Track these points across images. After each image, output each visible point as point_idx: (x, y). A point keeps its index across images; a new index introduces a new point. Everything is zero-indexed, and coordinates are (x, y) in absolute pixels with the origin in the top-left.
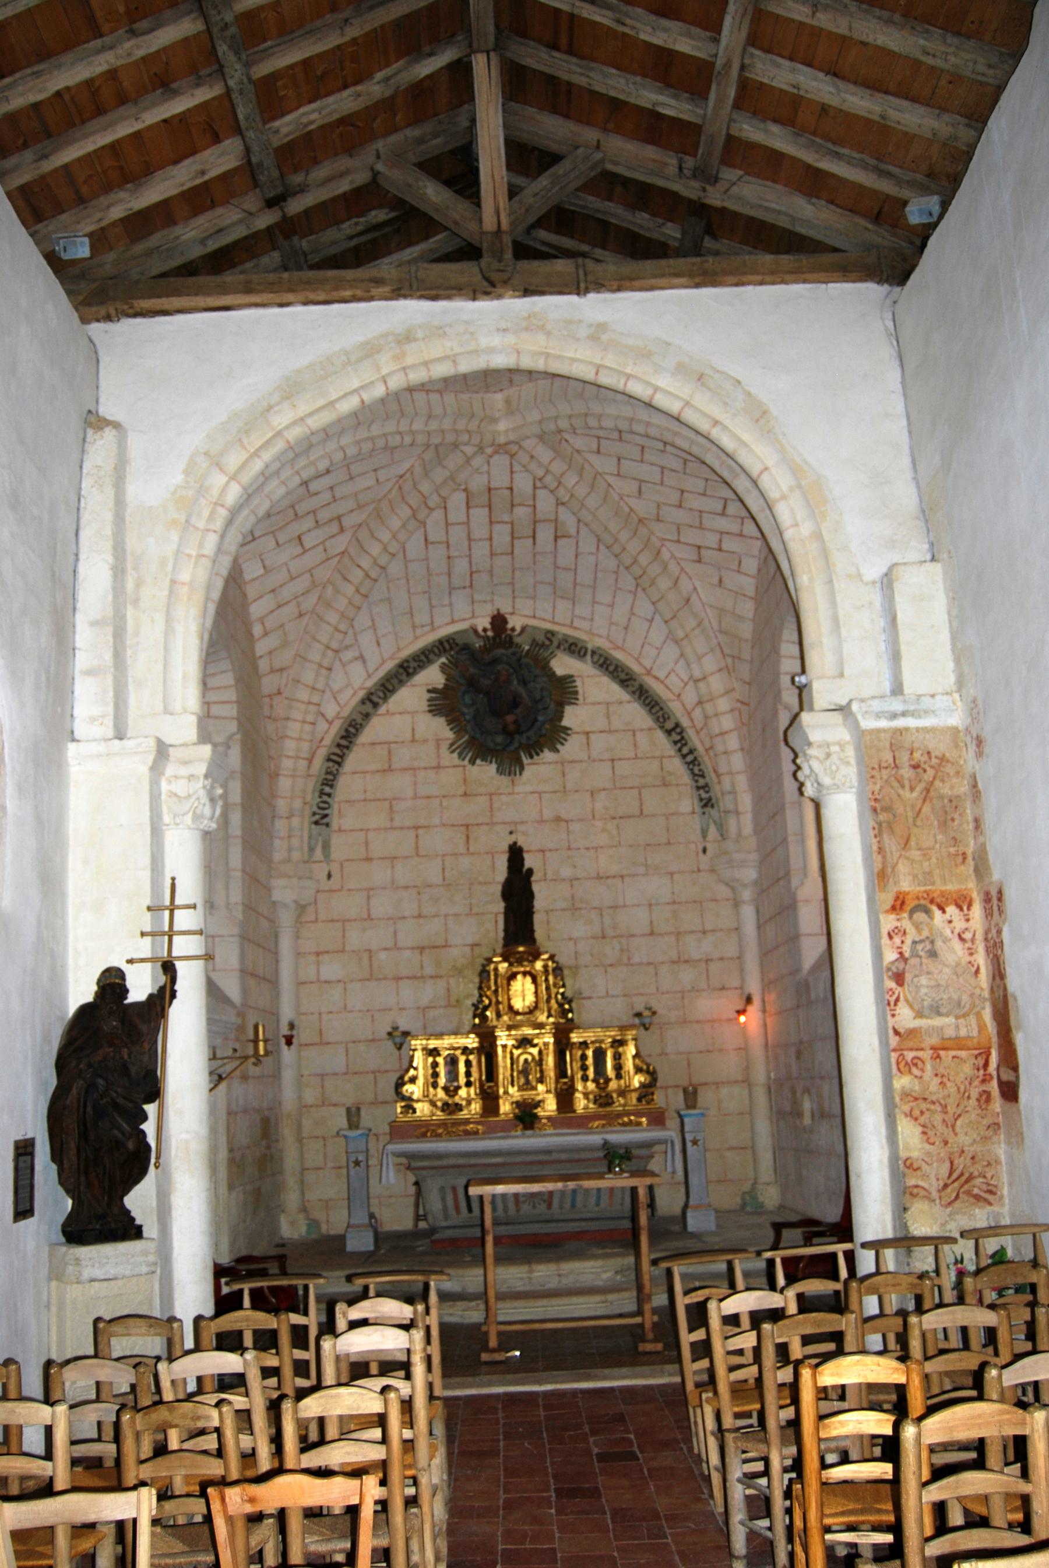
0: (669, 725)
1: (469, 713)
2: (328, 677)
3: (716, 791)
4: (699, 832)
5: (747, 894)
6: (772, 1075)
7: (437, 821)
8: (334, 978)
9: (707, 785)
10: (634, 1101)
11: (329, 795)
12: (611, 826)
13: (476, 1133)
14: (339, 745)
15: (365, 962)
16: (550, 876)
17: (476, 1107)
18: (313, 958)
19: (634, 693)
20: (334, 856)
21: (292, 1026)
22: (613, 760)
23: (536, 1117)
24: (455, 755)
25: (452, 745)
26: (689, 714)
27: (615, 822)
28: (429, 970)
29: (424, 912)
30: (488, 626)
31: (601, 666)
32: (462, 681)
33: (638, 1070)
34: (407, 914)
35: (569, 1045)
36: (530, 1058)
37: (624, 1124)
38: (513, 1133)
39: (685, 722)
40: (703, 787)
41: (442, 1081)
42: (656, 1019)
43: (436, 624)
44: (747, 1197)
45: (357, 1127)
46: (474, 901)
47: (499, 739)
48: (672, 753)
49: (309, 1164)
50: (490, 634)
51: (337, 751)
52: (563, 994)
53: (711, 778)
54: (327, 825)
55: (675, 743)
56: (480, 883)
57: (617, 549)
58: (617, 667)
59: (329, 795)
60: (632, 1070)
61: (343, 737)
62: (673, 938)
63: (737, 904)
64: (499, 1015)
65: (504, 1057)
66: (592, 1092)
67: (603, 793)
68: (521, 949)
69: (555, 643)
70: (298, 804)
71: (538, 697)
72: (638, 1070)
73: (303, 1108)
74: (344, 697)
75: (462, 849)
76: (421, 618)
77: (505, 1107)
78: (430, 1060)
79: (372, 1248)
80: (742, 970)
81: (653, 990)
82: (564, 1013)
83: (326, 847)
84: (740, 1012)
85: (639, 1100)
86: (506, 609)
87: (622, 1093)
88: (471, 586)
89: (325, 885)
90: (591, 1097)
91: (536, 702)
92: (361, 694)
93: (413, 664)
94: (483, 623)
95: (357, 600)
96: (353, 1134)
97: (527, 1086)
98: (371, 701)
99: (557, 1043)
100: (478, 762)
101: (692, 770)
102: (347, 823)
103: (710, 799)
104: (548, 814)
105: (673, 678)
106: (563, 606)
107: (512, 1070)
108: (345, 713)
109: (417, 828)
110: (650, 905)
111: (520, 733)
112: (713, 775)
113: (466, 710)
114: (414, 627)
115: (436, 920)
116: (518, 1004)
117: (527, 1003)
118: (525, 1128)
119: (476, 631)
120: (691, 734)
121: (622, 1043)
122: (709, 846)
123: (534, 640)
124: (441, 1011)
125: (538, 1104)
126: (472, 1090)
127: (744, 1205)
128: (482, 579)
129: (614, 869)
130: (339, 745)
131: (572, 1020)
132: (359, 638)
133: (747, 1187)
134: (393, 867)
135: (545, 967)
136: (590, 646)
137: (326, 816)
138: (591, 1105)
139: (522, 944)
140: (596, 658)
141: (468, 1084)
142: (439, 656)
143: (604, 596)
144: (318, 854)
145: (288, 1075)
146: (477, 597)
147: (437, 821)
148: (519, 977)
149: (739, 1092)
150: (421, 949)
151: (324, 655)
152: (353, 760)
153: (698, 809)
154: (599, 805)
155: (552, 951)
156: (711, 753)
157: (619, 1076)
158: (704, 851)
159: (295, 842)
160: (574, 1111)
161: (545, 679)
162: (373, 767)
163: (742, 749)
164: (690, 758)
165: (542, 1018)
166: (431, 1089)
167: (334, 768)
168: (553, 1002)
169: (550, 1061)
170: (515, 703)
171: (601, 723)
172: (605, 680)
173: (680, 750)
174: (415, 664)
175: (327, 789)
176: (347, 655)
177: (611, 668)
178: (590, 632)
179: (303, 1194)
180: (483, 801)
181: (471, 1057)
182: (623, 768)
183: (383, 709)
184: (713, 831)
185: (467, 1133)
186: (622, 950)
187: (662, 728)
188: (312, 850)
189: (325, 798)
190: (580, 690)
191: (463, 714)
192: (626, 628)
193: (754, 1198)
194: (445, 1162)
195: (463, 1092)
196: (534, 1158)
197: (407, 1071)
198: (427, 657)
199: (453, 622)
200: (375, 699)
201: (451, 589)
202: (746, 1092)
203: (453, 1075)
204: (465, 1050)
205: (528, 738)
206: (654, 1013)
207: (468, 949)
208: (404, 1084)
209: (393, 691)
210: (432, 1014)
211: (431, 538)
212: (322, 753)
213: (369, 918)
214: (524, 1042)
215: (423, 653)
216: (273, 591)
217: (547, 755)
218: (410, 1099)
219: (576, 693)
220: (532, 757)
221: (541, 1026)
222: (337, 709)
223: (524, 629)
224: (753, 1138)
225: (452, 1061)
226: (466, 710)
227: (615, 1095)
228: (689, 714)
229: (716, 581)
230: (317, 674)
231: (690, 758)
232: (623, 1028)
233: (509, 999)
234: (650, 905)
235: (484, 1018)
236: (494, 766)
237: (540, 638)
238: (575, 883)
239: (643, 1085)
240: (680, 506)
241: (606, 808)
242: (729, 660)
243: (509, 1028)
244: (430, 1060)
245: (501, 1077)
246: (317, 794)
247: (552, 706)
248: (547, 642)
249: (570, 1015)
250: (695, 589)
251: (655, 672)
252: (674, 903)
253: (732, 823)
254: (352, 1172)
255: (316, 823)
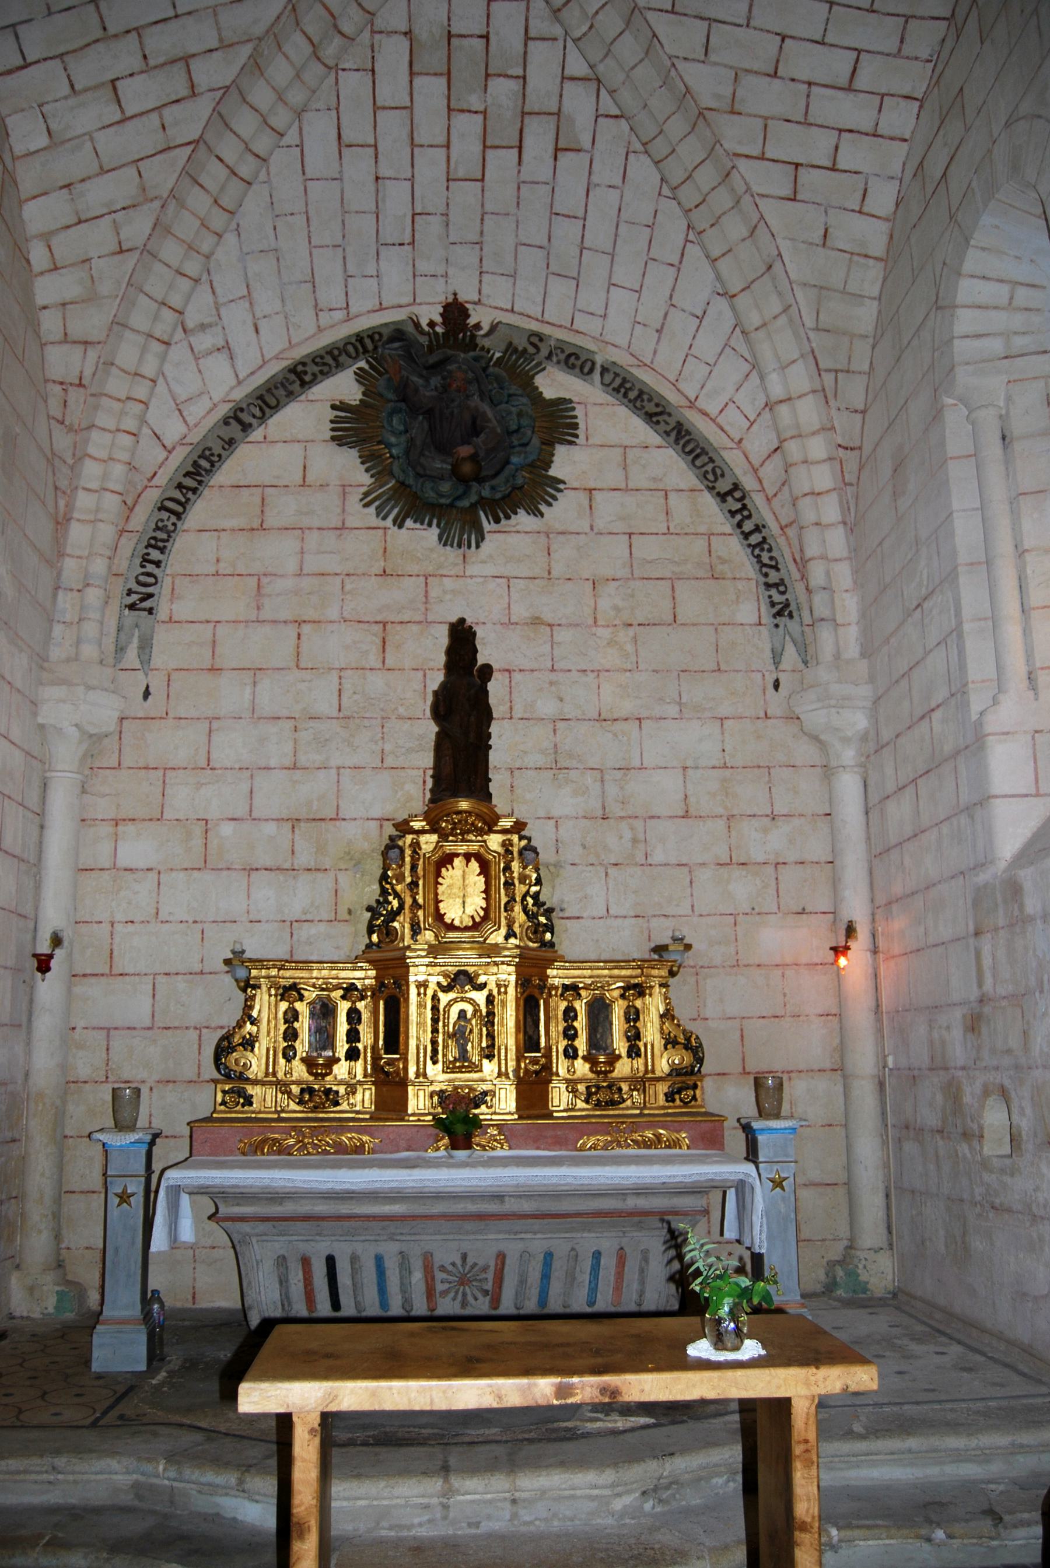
0: (723, 486)
1: (397, 445)
2: (163, 358)
3: (797, 592)
4: (768, 654)
5: (849, 755)
6: (890, 1061)
7: (333, 613)
8: (142, 864)
9: (782, 582)
10: (661, 1100)
11: (157, 564)
12: (624, 636)
13: (359, 1149)
14: (180, 486)
15: (197, 842)
16: (518, 712)
17: (364, 1099)
18: (107, 829)
19: (667, 433)
20: (157, 661)
21: (57, 941)
22: (630, 535)
23: (476, 1123)
24: (372, 509)
25: (366, 494)
26: (756, 471)
27: (631, 632)
28: (304, 858)
29: (303, 760)
30: (438, 319)
31: (617, 390)
32: (391, 396)
33: (670, 1042)
34: (272, 764)
35: (543, 986)
36: (469, 1009)
37: (646, 1144)
38: (431, 1153)
39: (748, 483)
40: (776, 585)
41: (302, 1046)
42: (689, 959)
43: (353, 310)
44: (840, 1273)
45: (132, 1128)
46: (388, 747)
47: (445, 487)
48: (728, 528)
49: (74, 1182)
50: (439, 330)
51: (177, 495)
52: (536, 896)
53: (790, 571)
54: (150, 611)
55: (733, 513)
56: (400, 718)
57: (660, 148)
58: (641, 393)
59: (157, 564)
60: (659, 1043)
61: (188, 474)
62: (721, 824)
63: (828, 772)
64: (416, 930)
65: (421, 1005)
66: (581, 1080)
67: (613, 585)
68: (464, 805)
69: (544, 352)
70: (99, 566)
71: (514, 427)
72: (670, 1042)
73: (71, 1085)
74: (196, 411)
75: (374, 660)
76: (332, 294)
77: (418, 1101)
78: (284, 1006)
79: (142, 1367)
80: (835, 883)
81: (685, 909)
82: (537, 931)
83: (146, 646)
84: (839, 951)
85: (670, 1097)
86: (467, 295)
87: (640, 1082)
88: (412, 243)
89: (140, 708)
90: (581, 1088)
91: (510, 433)
92: (224, 409)
93: (312, 368)
94: (430, 313)
95: (218, 220)
96: (117, 1140)
97: (463, 1063)
98: (239, 421)
99: (523, 982)
100: (409, 523)
101: (758, 557)
102: (183, 609)
103: (787, 605)
104: (520, 611)
105: (731, 411)
106: (559, 289)
107: (435, 1030)
108: (195, 437)
109: (299, 623)
110: (685, 768)
111: (480, 480)
112: (792, 567)
113: (393, 440)
114: (317, 309)
115: (322, 774)
116: (452, 912)
117: (470, 910)
118: (454, 1146)
119: (417, 325)
120: (758, 500)
121: (640, 990)
122: (783, 678)
123: (510, 344)
124: (322, 927)
125: (480, 1099)
126: (359, 1067)
127: (830, 1287)
128: (430, 229)
129: (627, 707)
130: (180, 486)
131: (551, 944)
132: (223, 312)
133: (836, 1252)
134: (255, 684)
135: (507, 845)
136: (599, 360)
137: (151, 596)
138: (580, 1104)
139: (467, 796)
140: (608, 378)
141: (352, 1055)
142: (356, 358)
143: (626, 273)
144: (131, 657)
145: (45, 1025)
146: (423, 267)
147: (333, 613)
148: (458, 862)
149: (827, 1086)
150: (295, 822)
151: (156, 318)
152: (199, 512)
153: (766, 619)
154: (604, 604)
155: (522, 813)
156: (791, 532)
157: (292, 1016)
158: (776, 685)
159: (90, 629)
160: (549, 1115)
161: (525, 400)
162: (234, 523)
163: (845, 523)
164: (755, 539)
165: (497, 937)
166: (282, 1061)
167: (169, 520)
168: (518, 908)
169: (508, 1018)
170: (475, 427)
171: (614, 477)
172: (624, 415)
173: (739, 525)
174: (316, 369)
175: (155, 555)
176: (205, 341)
177: (632, 395)
178: (600, 340)
179: (58, 1237)
180: (412, 586)
181: (360, 1005)
182: (647, 548)
183: (257, 434)
184: (791, 654)
185: (340, 1149)
186: (635, 841)
187: (711, 489)
188: (120, 650)
189: (150, 568)
190: (580, 421)
191: (389, 446)
192: (659, 331)
193: (852, 1274)
194: (288, 1208)
195: (341, 1070)
196: (472, 1208)
197: (240, 1025)
198: (335, 359)
199: (381, 308)
200: (246, 417)
201: (382, 244)
202: (839, 1088)
203: (324, 1037)
204: (349, 991)
205: (493, 488)
206: (688, 947)
207: (374, 825)
208: (232, 1049)
209: (276, 408)
210: (305, 932)
211: (348, 136)
212: (153, 496)
213: (209, 765)
214: (461, 980)
215: (330, 353)
216: (68, 186)
217: (523, 519)
218: (242, 1078)
219: (576, 426)
220: (497, 521)
221: (494, 950)
222: (183, 429)
223: (494, 328)
224: (849, 1168)
225: (324, 1011)
226: (393, 440)
227: (625, 1087)
228: (756, 471)
229: (817, 236)
230: (144, 350)
231: (755, 539)
232: (642, 964)
233: (437, 902)
234: (685, 768)
235: (389, 934)
236: (435, 531)
237: (521, 343)
238: (560, 725)
239: (676, 1072)
240: (775, 75)
241: (617, 609)
242: (828, 379)
243: (433, 950)
244: (284, 1006)
245: (413, 1043)
246: (138, 561)
247: (536, 442)
248: (531, 350)
249: (548, 936)
250: (780, 255)
251: (701, 404)
252: (725, 767)
253: (825, 636)
254: (114, 1212)
255: (132, 607)
